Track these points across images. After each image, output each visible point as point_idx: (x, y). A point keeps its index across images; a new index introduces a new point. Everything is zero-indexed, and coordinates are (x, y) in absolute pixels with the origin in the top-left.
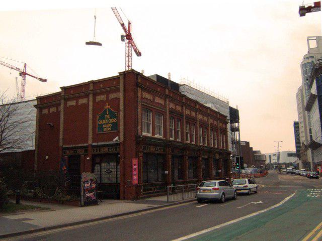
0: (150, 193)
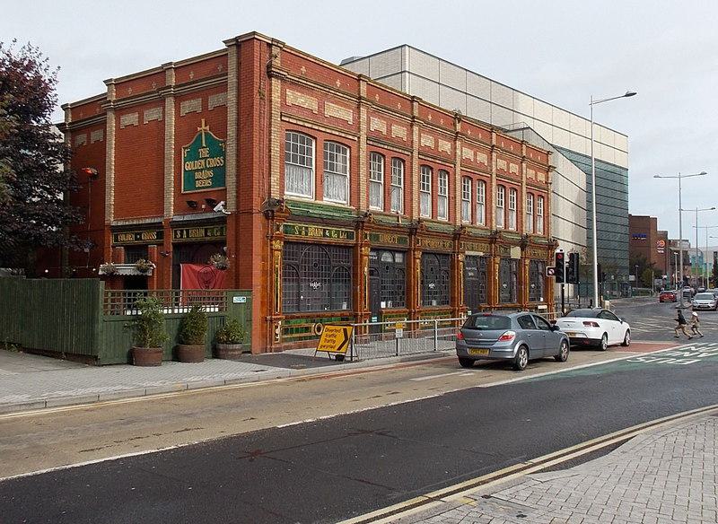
0: (305, 338)
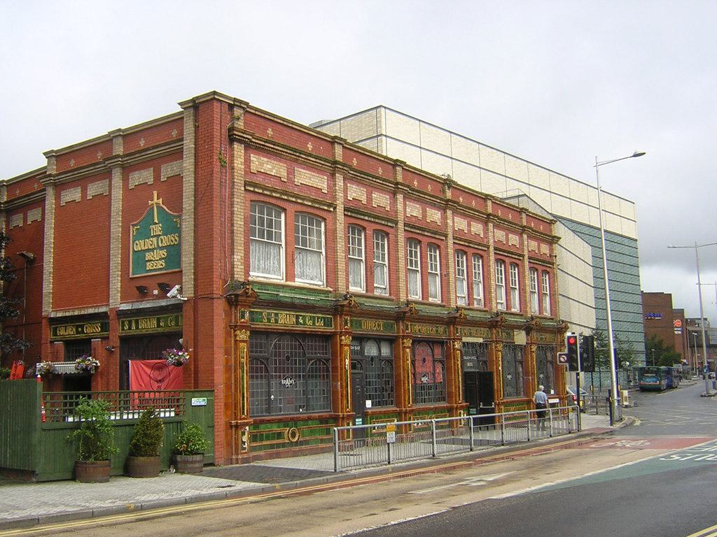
0: (278, 446)
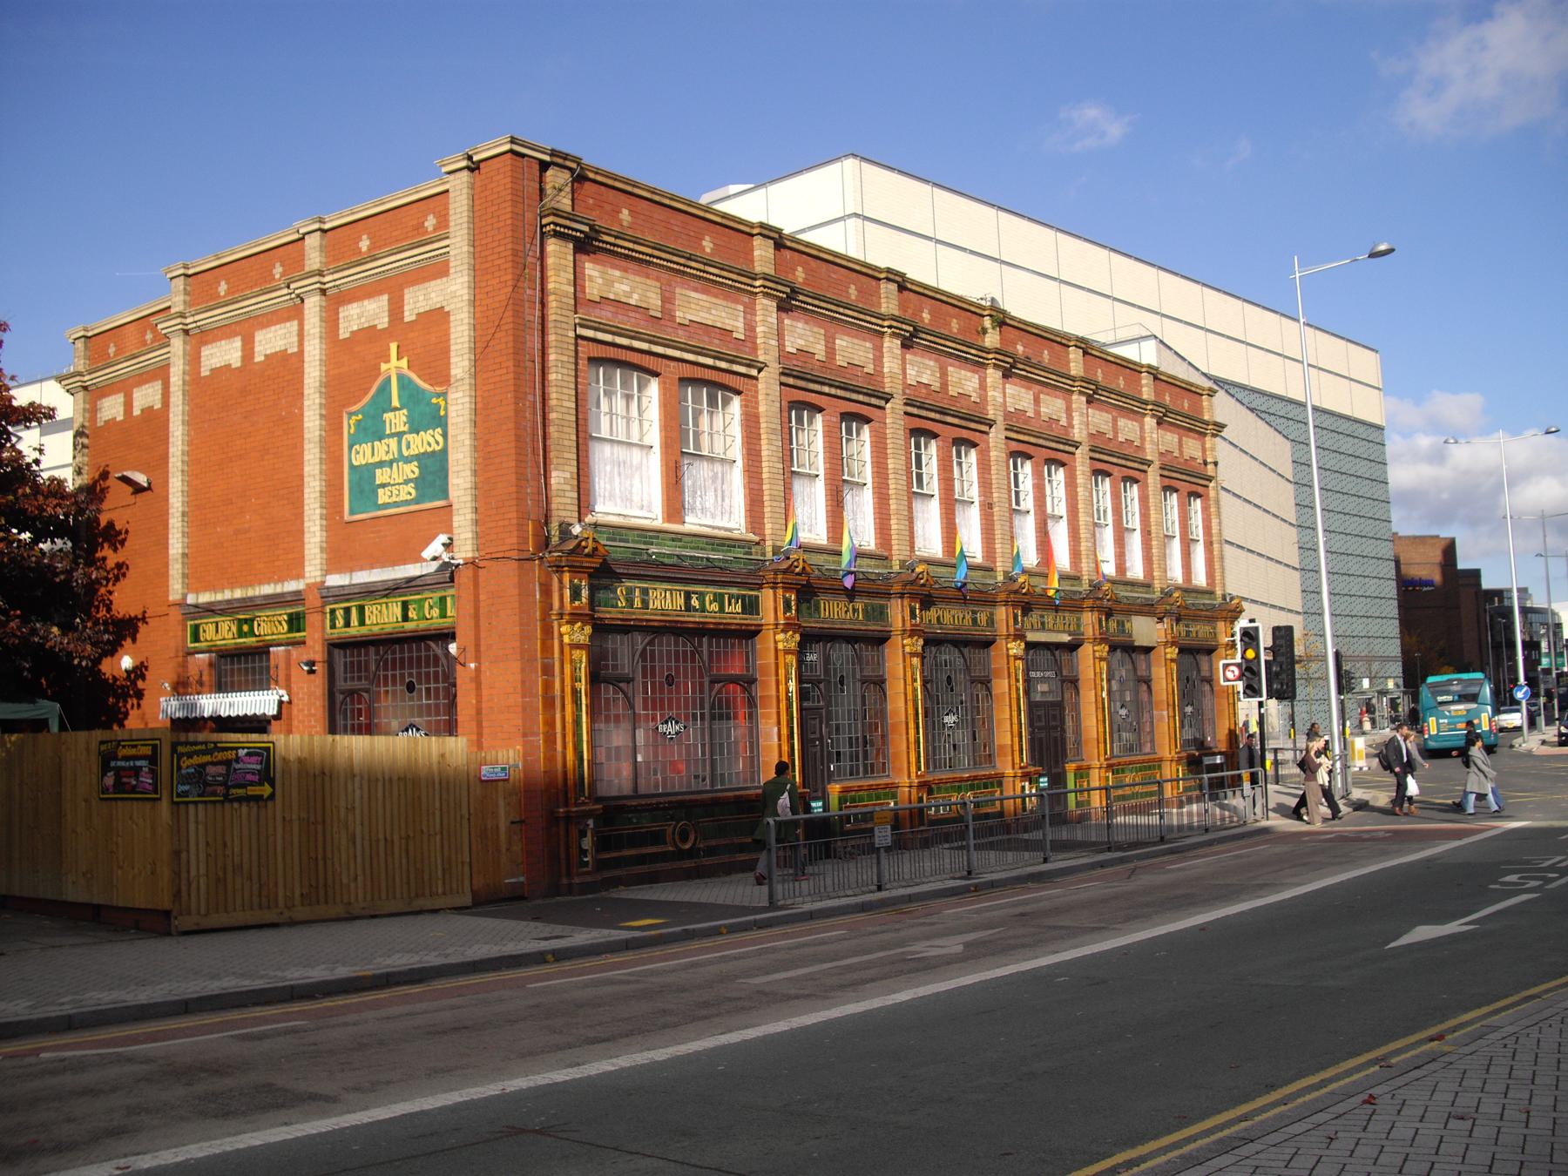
0: (654, 858)
